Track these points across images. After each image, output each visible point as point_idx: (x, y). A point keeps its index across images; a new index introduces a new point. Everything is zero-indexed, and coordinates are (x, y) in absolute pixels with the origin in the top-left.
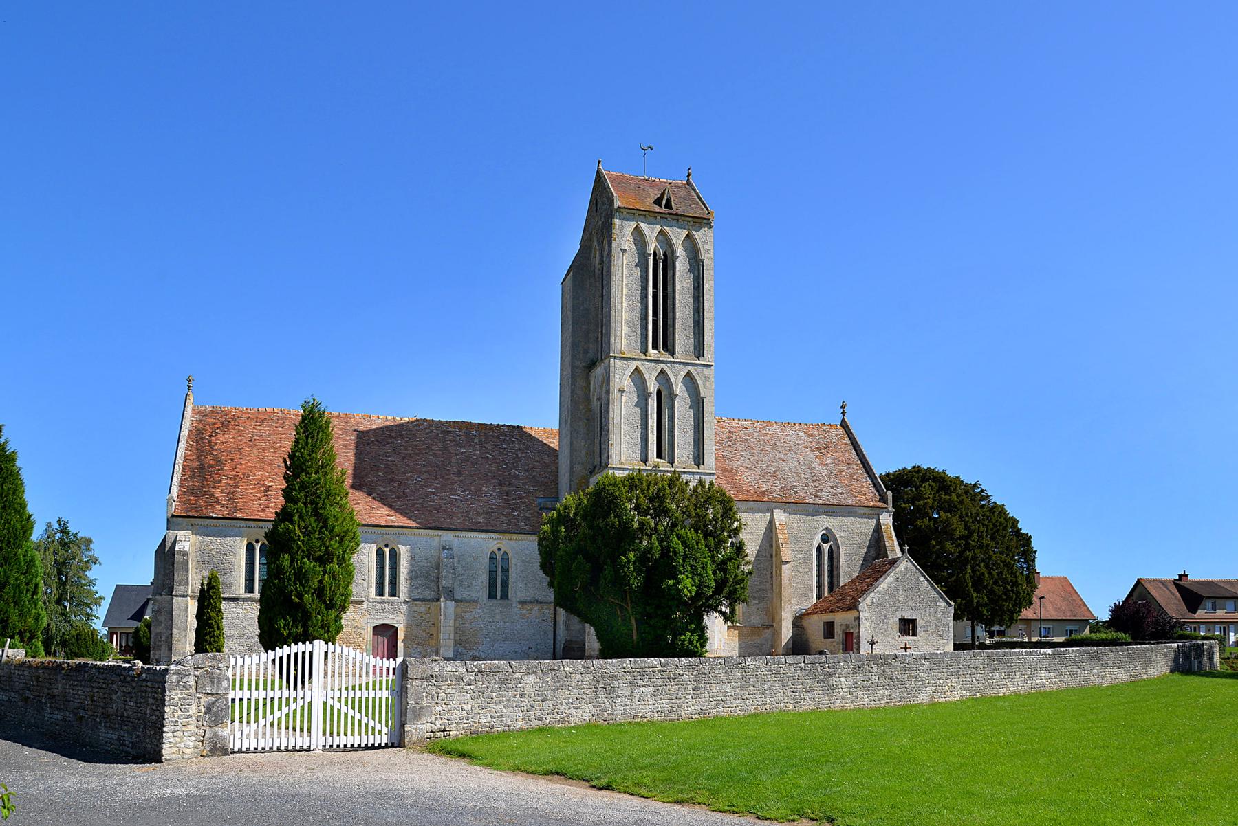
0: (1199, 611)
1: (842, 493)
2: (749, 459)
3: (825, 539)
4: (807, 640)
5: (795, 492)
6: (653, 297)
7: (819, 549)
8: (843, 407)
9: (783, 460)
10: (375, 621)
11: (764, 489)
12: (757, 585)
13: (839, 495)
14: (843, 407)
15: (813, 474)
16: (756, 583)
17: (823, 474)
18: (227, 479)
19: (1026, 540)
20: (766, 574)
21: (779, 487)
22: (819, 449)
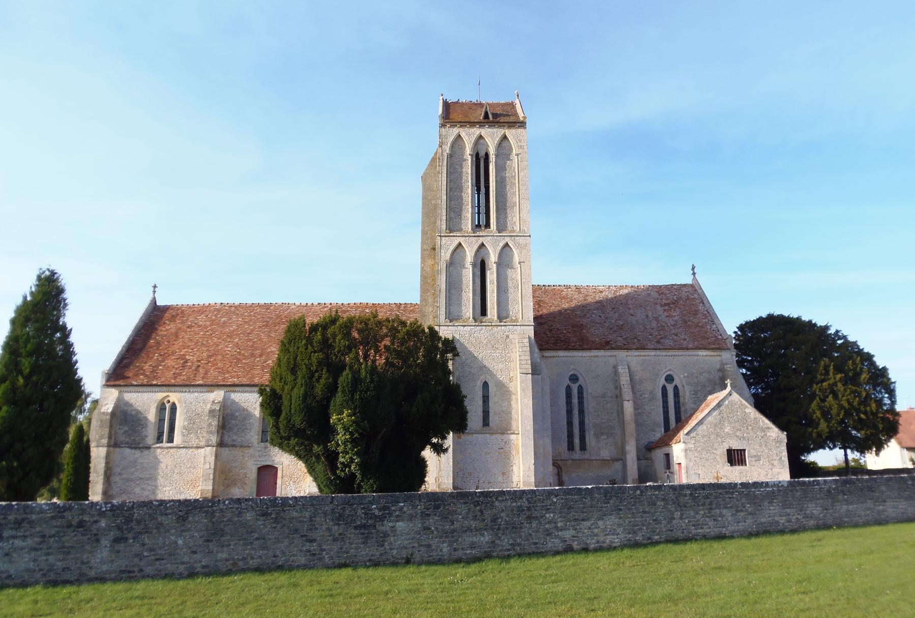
0: (110, 410)
1: (685, 339)
2: (600, 316)
3: (669, 379)
4: (655, 471)
5: (639, 340)
6: (480, 181)
7: (664, 389)
8: (693, 268)
9: (632, 315)
10: (259, 463)
11: (608, 340)
12: (605, 422)
13: (682, 341)
14: (693, 268)
15: (659, 325)
16: (603, 421)
17: (669, 324)
18: (308, 367)
19: (883, 373)
20: (613, 413)
21: (624, 337)
22: (668, 304)
